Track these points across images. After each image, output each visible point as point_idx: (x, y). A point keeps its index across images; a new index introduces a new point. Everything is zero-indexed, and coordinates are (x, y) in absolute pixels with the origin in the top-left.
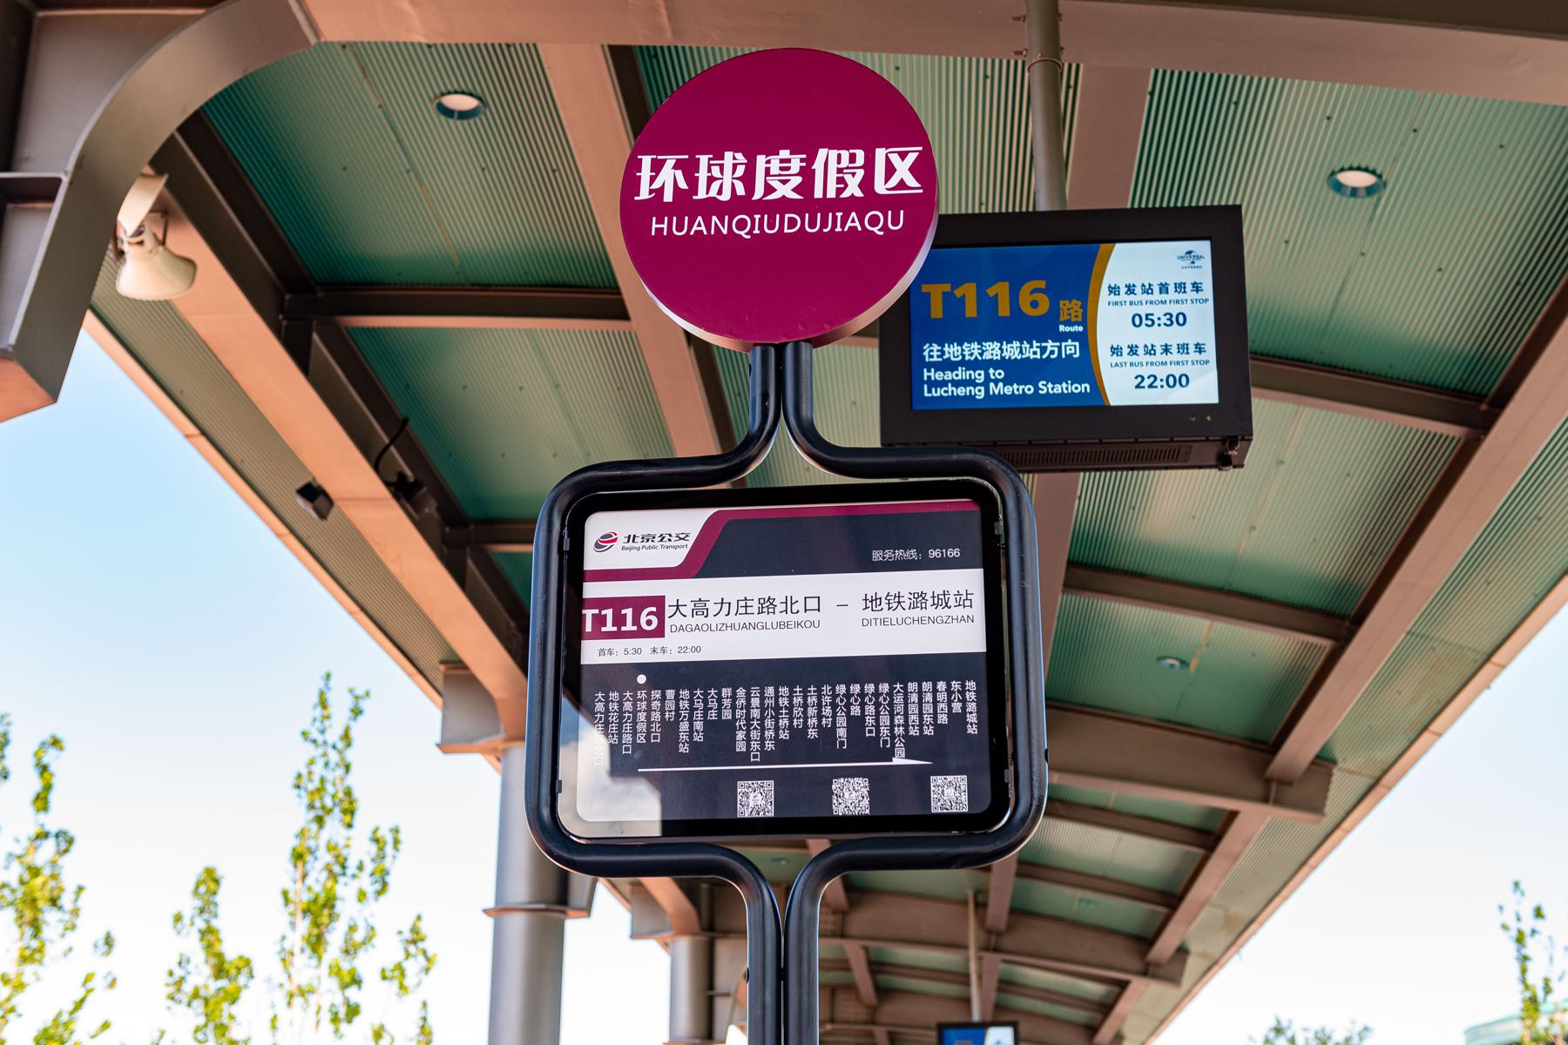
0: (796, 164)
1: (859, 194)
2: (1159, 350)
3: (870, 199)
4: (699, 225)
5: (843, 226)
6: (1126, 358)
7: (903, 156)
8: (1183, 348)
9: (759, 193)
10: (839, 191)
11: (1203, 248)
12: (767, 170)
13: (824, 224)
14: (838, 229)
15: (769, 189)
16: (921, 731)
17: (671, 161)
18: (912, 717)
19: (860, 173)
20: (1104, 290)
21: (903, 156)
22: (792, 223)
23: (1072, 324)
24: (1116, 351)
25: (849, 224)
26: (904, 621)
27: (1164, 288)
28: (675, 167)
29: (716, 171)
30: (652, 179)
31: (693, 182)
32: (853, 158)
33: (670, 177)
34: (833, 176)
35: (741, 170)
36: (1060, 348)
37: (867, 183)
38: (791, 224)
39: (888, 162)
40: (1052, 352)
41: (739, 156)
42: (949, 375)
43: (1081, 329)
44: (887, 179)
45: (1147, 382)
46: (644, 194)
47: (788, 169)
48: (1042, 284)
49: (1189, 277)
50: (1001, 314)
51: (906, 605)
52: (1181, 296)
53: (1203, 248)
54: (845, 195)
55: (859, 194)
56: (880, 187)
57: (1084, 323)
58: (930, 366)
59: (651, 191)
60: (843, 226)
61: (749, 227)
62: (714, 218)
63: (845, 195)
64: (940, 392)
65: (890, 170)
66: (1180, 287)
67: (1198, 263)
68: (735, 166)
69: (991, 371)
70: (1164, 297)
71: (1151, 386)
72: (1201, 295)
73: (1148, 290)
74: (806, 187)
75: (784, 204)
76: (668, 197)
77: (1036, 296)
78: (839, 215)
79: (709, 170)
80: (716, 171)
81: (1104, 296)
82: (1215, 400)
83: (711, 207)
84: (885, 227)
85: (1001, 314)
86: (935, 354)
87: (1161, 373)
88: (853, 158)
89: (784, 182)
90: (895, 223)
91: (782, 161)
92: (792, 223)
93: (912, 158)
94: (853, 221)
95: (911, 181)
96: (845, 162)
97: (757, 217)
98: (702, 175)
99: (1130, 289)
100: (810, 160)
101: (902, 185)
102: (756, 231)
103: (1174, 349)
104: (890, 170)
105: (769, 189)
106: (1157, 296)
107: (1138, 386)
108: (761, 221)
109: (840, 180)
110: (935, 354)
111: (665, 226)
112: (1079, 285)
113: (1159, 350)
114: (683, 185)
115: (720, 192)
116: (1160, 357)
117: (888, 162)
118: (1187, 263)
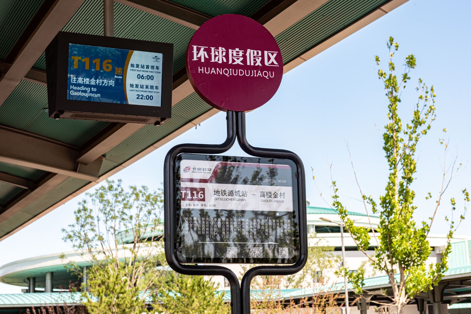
0: (241, 54)
1: (260, 65)
2: (145, 87)
3: (264, 68)
4: (213, 71)
5: (257, 75)
6: (135, 88)
7: (272, 54)
8: (152, 87)
9: (230, 62)
10: (255, 63)
11: (160, 55)
12: (232, 54)
13: (251, 74)
14: (255, 76)
15: (233, 61)
16: (201, 233)
17: (202, 49)
18: (203, 228)
19: (260, 58)
20: (130, 65)
21: (272, 54)
22: (241, 73)
23: (119, 76)
24: (132, 86)
25: (258, 74)
26: (226, 199)
27: (148, 67)
28: (204, 50)
29: (217, 53)
30: (197, 54)
31: (210, 56)
32: (258, 53)
33: (203, 54)
34: (252, 59)
35: (224, 54)
36: (108, 82)
37: (263, 62)
38: (241, 73)
39: (268, 55)
40: (106, 84)
41: (224, 49)
42: (79, 88)
43: (121, 77)
44: (268, 61)
45: (140, 97)
46: (195, 59)
47: (239, 55)
48: (110, 61)
49: (155, 64)
50: (86, 68)
51: (227, 194)
52: (153, 70)
53: (160, 55)
54: (256, 65)
55: (260, 65)
56: (267, 64)
57: (122, 76)
58: (72, 84)
59: (197, 58)
60: (257, 75)
61: (229, 73)
62: (218, 69)
63: (256, 65)
64: (76, 94)
65: (269, 59)
66: (153, 67)
67: (158, 60)
68: (222, 52)
69: (92, 88)
70: (147, 70)
71: (141, 98)
72: (158, 71)
73: (143, 67)
74: (244, 61)
75: (238, 66)
76: (203, 60)
77: (109, 65)
78: (255, 71)
79: (215, 53)
80: (217, 53)
81: (129, 67)
82: (159, 105)
83: (216, 65)
84: (269, 77)
85: (86, 68)
86: (75, 80)
87: (145, 94)
88: (258, 53)
89: (238, 59)
90: (272, 76)
91: (237, 52)
92: (241, 73)
93: (275, 55)
94: (259, 74)
95: (275, 63)
96: (256, 54)
97: (231, 70)
98: (213, 54)
99: (143, 67)
100: (245, 52)
101: (273, 63)
102: (231, 74)
103: (149, 87)
104: (269, 59)
105: (233, 61)
106: (145, 69)
107: (137, 98)
108: (232, 71)
109: (255, 60)
110: (75, 80)
111: (203, 70)
112: (122, 63)
113: (145, 87)
114: (207, 57)
115: (219, 60)
116: (145, 89)
117: (268, 55)
118: (155, 60)
